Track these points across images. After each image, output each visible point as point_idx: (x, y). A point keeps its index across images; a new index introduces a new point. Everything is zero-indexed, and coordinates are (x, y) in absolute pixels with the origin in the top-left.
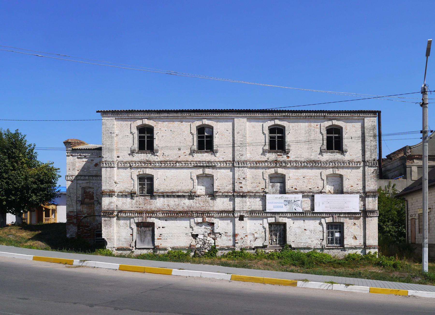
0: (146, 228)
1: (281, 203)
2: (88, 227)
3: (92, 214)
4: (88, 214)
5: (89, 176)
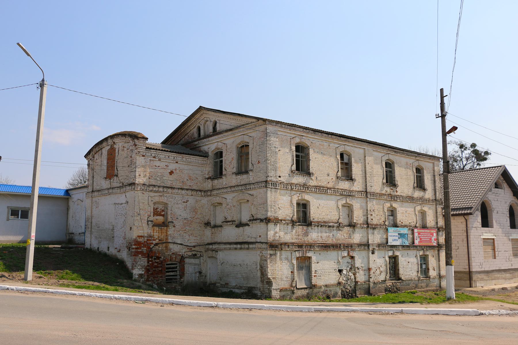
0: (305, 264)
1: (396, 236)
2: (158, 258)
3: (164, 241)
4: (159, 240)
5: (164, 187)
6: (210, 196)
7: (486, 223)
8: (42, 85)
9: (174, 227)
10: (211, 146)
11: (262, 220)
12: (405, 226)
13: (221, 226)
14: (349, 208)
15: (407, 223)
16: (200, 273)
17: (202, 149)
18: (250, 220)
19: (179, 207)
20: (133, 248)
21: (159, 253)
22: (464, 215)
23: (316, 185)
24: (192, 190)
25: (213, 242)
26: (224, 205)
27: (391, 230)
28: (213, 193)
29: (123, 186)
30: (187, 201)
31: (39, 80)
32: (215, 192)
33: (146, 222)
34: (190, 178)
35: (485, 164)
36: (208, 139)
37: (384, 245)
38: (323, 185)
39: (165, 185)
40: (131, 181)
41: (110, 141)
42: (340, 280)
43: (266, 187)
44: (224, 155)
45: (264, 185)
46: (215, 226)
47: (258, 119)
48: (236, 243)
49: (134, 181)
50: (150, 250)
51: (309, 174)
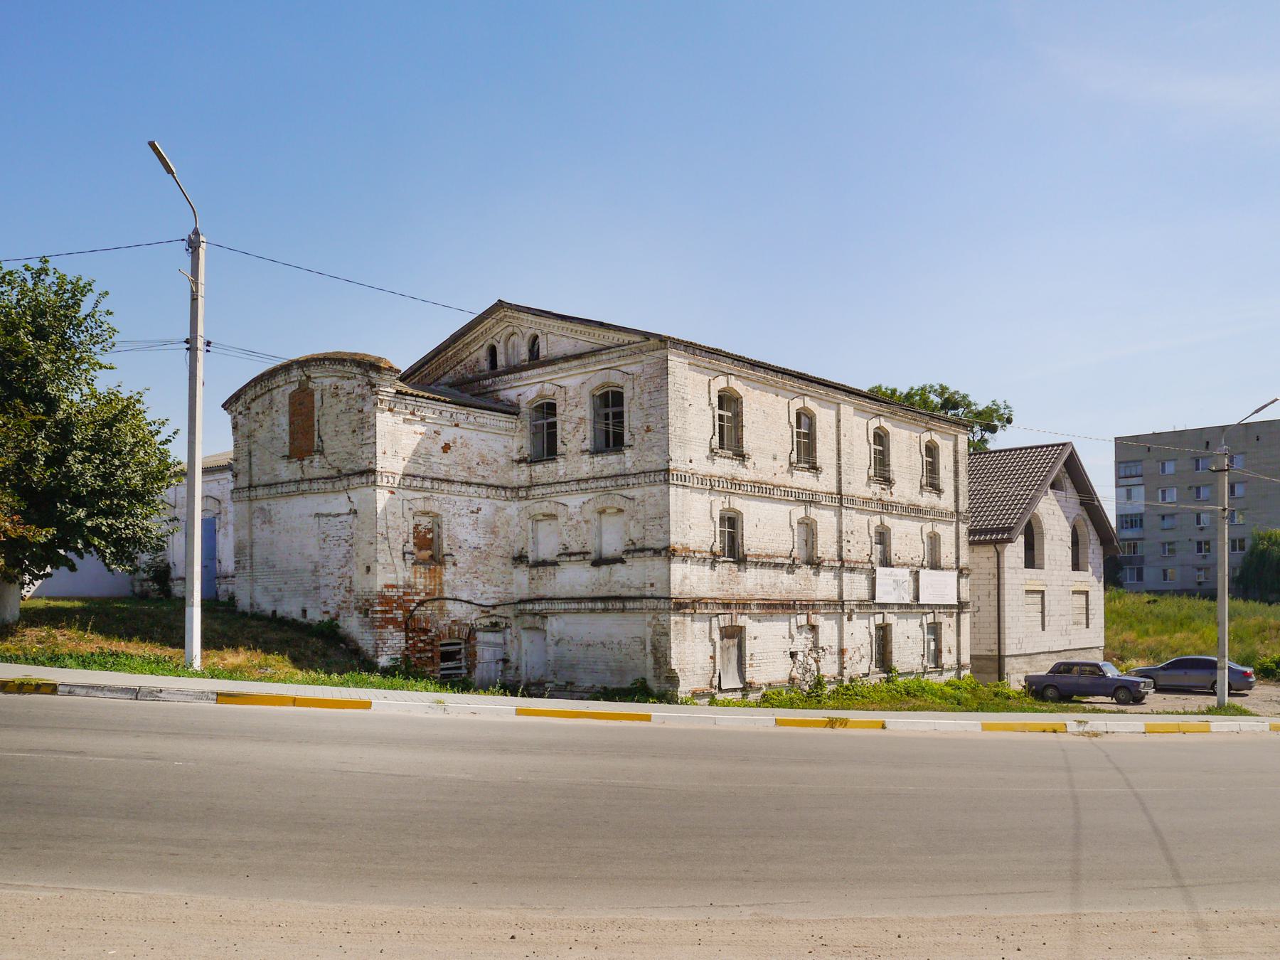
2: (426, 631)
3: (437, 595)
5: (433, 479)
6: (526, 498)
7: (1031, 560)
8: (193, 245)
9: (455, 564)
10: (527, 389)
11: (657, 552)
12: (905, 565)
13: (555, 564)
14: (809, 528)
15: (908, 560)
16: (505, 661)
17: (502, 395)
18: (627, 552)
19: (464, 524)
20: (376, 612)
21: (427, 622)
22: (996, 542)
23: (754, 479)
24: (489, 486)
25: (533, 596)
26: (562, 520)
27: (881, 571)
28: (533, 492)
29: (340, 475)
30: (479, 509)
31: (187, 232)
32: (537, 492)
33: (400, 554)
34: (483, 461)
35: (998, 441)
36: (517, 375)
37: (870, 604)
38: (765, 479)
39: (435, 476)
40: (364, 465)
41: (296, 374)
42: (793, 674)
43: (667, 482)
44: (559, 410)
45: (661, 477)
46: (544, 563)
47: (647, 336)
48: (594, 599)
49: (372, 466)
50: (410, 615)
51: (741, 456)
